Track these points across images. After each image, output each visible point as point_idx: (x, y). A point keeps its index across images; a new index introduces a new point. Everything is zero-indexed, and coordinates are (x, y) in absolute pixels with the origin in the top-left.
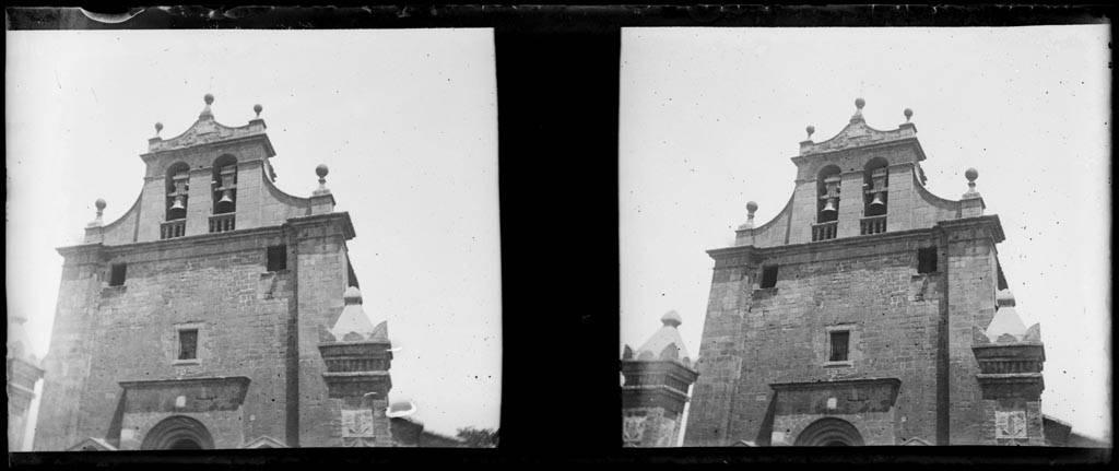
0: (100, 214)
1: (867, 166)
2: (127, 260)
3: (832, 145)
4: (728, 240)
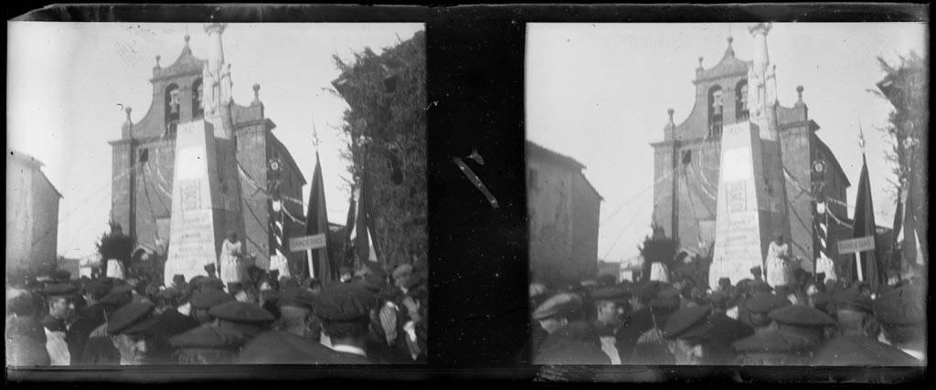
1: (194, 84)
2: (690, 147)
4: (661, 138)
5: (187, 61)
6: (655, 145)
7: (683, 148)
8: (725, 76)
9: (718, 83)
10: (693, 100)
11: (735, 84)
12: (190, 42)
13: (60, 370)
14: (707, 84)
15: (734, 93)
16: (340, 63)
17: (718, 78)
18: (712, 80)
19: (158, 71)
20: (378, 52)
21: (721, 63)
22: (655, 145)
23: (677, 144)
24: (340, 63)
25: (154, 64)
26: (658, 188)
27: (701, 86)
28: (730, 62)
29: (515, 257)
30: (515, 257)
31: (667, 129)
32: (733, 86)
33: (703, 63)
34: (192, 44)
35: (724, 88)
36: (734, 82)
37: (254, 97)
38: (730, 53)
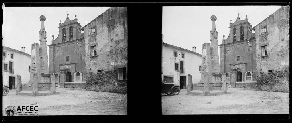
3: (235, 24)
8: (237, 25)
12: (69, 16)
17: (65, 26)
19: (60, 25)
27: (60, 28)
32: (68, 28)
36: (239, 27)
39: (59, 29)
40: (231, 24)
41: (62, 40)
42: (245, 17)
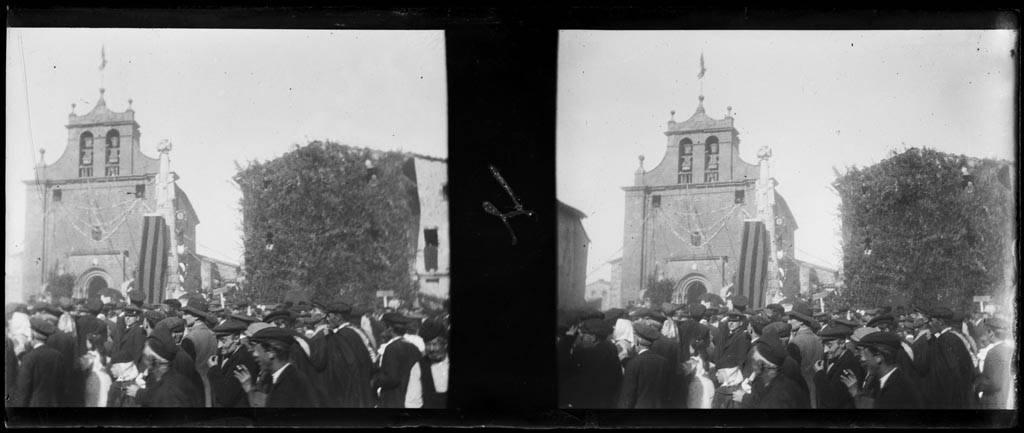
0: (642, 163)
5: (701, 118)
6: (627, 189)
7: (653, 194)
9: (716, 134)
10: (664, 150)
11: (705, 139)
13: (761, 293)
14: (79, 129)
15: (704, 147)
16: (837, 172)
17: (689, 132)
18: (683, 133)
20: (860, 169)
21: (94, 111)
22: (627, 189)
23: (648, 190)
24: (837, 172)
25: (70, 110)
26: (629, 228)
27: (74, 130)
28: (101, 111)
29: (981, 394)
30: (981, 394)
31: (637, 174)
33: (76, 109)
34: (107, 97)
35: (695, 141)
37: (639, 165)
38: (701, 110)
39: (666, 138)
40: (72, 115)
41: (676, 178)
42: (126, 106)
